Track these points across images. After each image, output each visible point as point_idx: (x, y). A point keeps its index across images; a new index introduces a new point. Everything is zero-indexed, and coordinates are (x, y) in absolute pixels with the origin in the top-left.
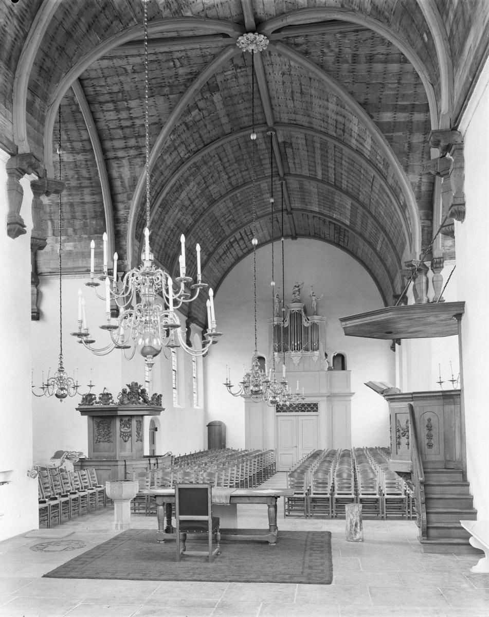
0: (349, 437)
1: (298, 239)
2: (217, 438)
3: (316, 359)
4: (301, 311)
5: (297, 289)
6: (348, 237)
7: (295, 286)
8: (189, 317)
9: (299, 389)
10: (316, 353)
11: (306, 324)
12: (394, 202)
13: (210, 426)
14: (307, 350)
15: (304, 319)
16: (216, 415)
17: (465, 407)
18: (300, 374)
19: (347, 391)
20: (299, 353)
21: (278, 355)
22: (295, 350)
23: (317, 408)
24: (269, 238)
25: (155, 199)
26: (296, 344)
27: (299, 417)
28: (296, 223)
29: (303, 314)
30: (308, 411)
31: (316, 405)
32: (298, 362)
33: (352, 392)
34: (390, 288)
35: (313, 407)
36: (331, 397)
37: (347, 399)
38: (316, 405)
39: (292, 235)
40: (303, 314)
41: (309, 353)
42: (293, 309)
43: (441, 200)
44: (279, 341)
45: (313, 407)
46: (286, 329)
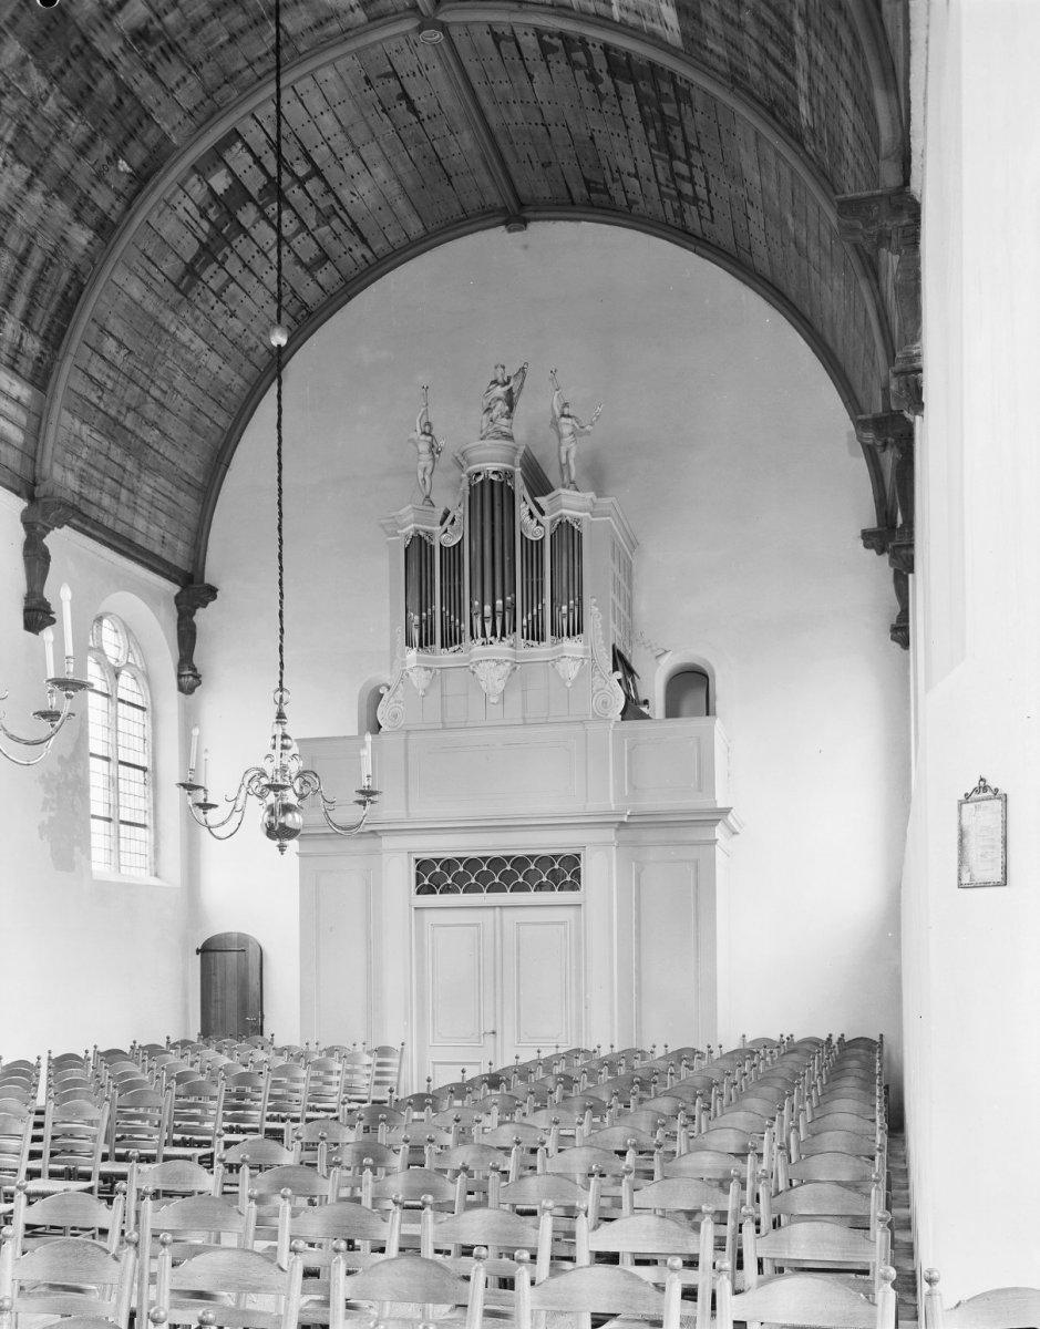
0: (706, 988)
1: (532, 226)
2: (232, 997)
3: (570, 670)
4: (509, 475)
5: (500, 391)
6: (704, 169)
7: (495, 382)
8: (32, 498)
9: (533, 801)
10: (570, 645)
11: (534, 532)
12: (868, 51)
13: (207, 950)
14: (535, 635)
15: (522, 510)
16: (226, 917)
17: (177, 755)
18: (522, 732)
19: (699, 802)
20: (500, 648)
21: (419, 660)
22: (484, 635)
23: (577, 874)
24: (415, 227)
25: (128, 207)
26: (488, 608)
27: (507, 914)
28: (493, 119)
29: (520, 489)
30: (540, 887)
31: (573, 861)
32: (500, 686)
33: (721, 805)
34: (898, 27)
35: (562, 872)
36: (632, 827)
37: (698, 834)
38: (573, 861)
39: (505, 210)
40: (520, 489)
41: (543, 650)
42: (475, 467)
43: (899, 514)
44: (424, 603)
45: (562, 872)
46: (452, 555)
